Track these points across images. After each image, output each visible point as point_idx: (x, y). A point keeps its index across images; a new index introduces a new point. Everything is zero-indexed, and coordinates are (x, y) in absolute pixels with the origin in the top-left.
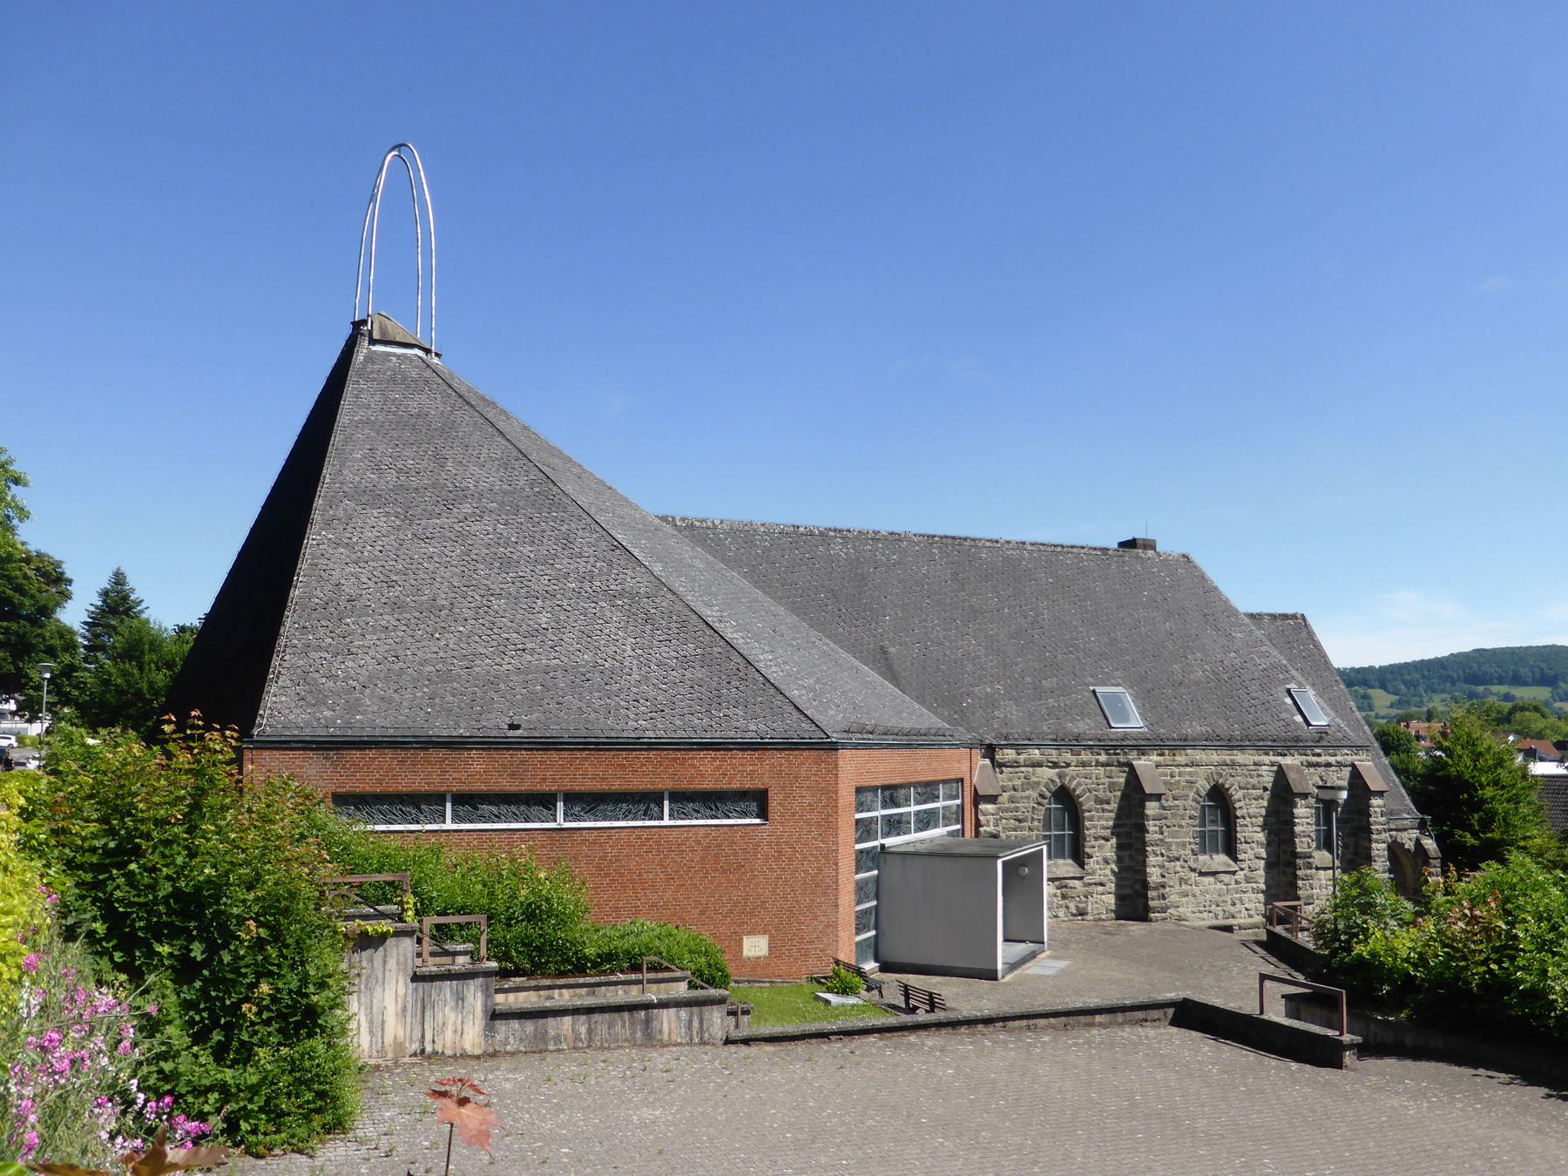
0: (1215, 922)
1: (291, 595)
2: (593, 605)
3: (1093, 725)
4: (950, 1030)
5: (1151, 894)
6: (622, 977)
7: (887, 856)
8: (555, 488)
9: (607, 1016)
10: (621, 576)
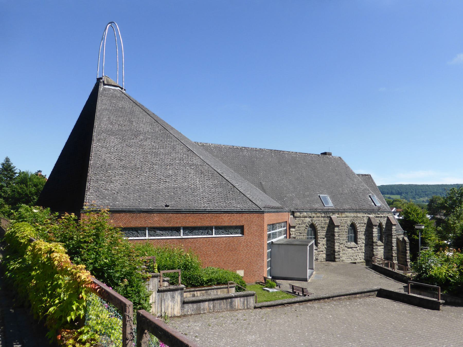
0: (351, 261)
1: (90, 163)
2: (185, 168)
3: (320, 206)
4: (318, 301)
5: (336, 254)
6: (216, 287)
7: (273, 245)
8: (167, 132)
9: (219, 301)
10: (192, 159)
